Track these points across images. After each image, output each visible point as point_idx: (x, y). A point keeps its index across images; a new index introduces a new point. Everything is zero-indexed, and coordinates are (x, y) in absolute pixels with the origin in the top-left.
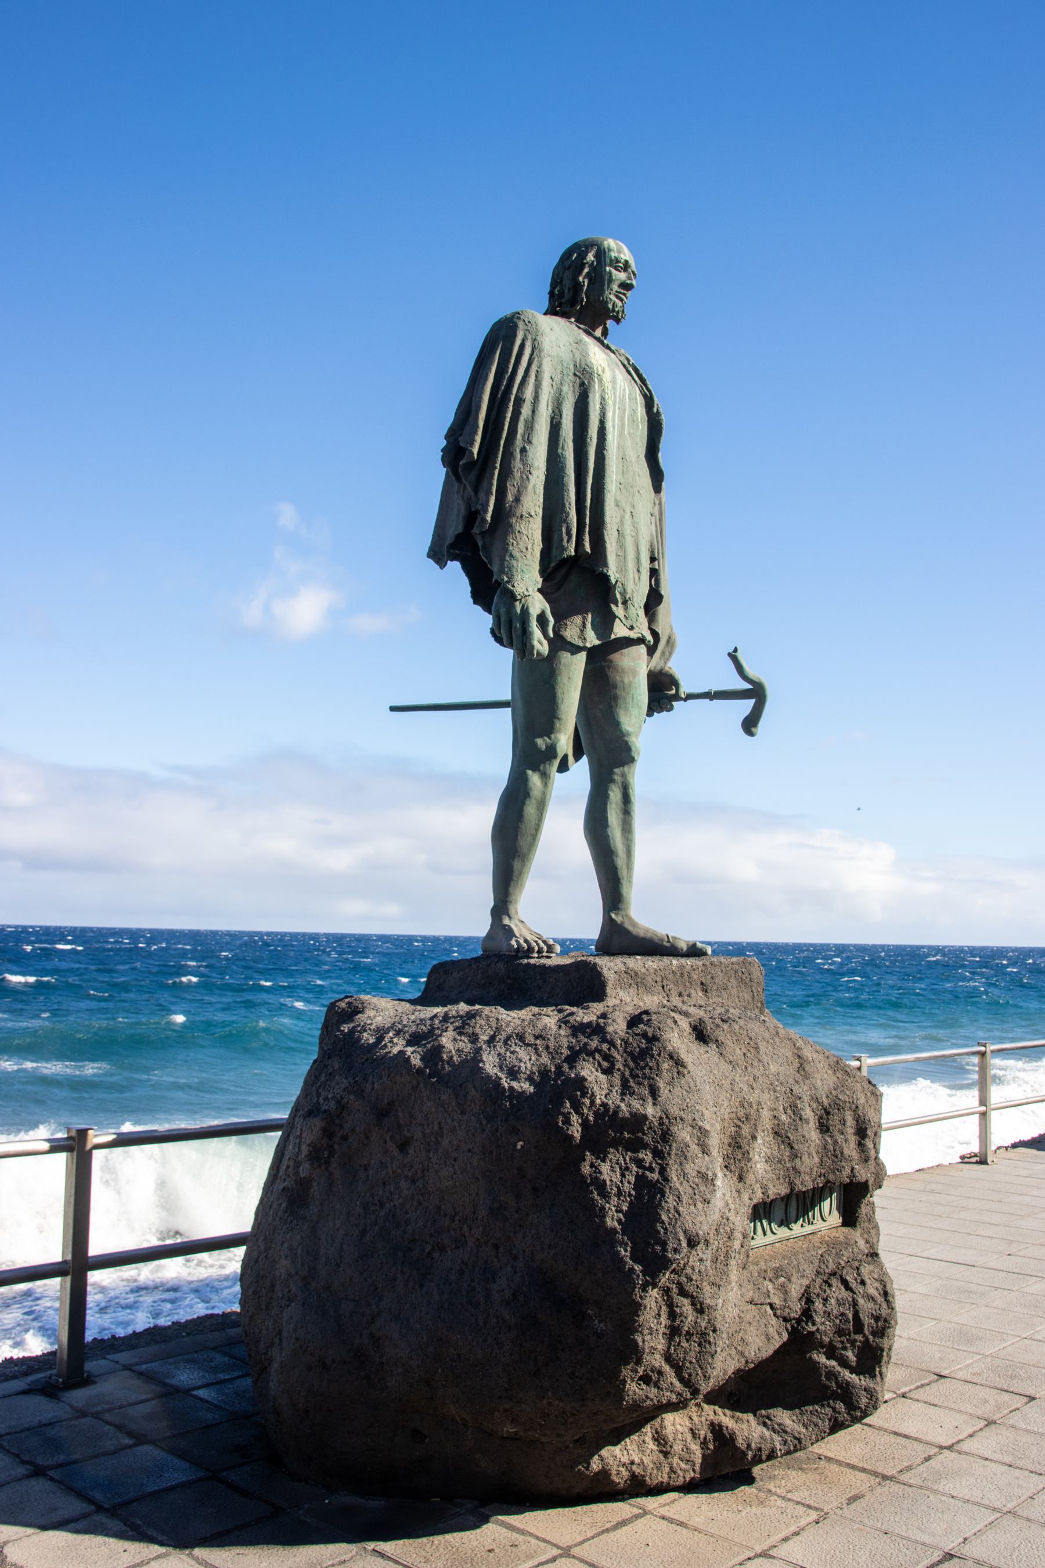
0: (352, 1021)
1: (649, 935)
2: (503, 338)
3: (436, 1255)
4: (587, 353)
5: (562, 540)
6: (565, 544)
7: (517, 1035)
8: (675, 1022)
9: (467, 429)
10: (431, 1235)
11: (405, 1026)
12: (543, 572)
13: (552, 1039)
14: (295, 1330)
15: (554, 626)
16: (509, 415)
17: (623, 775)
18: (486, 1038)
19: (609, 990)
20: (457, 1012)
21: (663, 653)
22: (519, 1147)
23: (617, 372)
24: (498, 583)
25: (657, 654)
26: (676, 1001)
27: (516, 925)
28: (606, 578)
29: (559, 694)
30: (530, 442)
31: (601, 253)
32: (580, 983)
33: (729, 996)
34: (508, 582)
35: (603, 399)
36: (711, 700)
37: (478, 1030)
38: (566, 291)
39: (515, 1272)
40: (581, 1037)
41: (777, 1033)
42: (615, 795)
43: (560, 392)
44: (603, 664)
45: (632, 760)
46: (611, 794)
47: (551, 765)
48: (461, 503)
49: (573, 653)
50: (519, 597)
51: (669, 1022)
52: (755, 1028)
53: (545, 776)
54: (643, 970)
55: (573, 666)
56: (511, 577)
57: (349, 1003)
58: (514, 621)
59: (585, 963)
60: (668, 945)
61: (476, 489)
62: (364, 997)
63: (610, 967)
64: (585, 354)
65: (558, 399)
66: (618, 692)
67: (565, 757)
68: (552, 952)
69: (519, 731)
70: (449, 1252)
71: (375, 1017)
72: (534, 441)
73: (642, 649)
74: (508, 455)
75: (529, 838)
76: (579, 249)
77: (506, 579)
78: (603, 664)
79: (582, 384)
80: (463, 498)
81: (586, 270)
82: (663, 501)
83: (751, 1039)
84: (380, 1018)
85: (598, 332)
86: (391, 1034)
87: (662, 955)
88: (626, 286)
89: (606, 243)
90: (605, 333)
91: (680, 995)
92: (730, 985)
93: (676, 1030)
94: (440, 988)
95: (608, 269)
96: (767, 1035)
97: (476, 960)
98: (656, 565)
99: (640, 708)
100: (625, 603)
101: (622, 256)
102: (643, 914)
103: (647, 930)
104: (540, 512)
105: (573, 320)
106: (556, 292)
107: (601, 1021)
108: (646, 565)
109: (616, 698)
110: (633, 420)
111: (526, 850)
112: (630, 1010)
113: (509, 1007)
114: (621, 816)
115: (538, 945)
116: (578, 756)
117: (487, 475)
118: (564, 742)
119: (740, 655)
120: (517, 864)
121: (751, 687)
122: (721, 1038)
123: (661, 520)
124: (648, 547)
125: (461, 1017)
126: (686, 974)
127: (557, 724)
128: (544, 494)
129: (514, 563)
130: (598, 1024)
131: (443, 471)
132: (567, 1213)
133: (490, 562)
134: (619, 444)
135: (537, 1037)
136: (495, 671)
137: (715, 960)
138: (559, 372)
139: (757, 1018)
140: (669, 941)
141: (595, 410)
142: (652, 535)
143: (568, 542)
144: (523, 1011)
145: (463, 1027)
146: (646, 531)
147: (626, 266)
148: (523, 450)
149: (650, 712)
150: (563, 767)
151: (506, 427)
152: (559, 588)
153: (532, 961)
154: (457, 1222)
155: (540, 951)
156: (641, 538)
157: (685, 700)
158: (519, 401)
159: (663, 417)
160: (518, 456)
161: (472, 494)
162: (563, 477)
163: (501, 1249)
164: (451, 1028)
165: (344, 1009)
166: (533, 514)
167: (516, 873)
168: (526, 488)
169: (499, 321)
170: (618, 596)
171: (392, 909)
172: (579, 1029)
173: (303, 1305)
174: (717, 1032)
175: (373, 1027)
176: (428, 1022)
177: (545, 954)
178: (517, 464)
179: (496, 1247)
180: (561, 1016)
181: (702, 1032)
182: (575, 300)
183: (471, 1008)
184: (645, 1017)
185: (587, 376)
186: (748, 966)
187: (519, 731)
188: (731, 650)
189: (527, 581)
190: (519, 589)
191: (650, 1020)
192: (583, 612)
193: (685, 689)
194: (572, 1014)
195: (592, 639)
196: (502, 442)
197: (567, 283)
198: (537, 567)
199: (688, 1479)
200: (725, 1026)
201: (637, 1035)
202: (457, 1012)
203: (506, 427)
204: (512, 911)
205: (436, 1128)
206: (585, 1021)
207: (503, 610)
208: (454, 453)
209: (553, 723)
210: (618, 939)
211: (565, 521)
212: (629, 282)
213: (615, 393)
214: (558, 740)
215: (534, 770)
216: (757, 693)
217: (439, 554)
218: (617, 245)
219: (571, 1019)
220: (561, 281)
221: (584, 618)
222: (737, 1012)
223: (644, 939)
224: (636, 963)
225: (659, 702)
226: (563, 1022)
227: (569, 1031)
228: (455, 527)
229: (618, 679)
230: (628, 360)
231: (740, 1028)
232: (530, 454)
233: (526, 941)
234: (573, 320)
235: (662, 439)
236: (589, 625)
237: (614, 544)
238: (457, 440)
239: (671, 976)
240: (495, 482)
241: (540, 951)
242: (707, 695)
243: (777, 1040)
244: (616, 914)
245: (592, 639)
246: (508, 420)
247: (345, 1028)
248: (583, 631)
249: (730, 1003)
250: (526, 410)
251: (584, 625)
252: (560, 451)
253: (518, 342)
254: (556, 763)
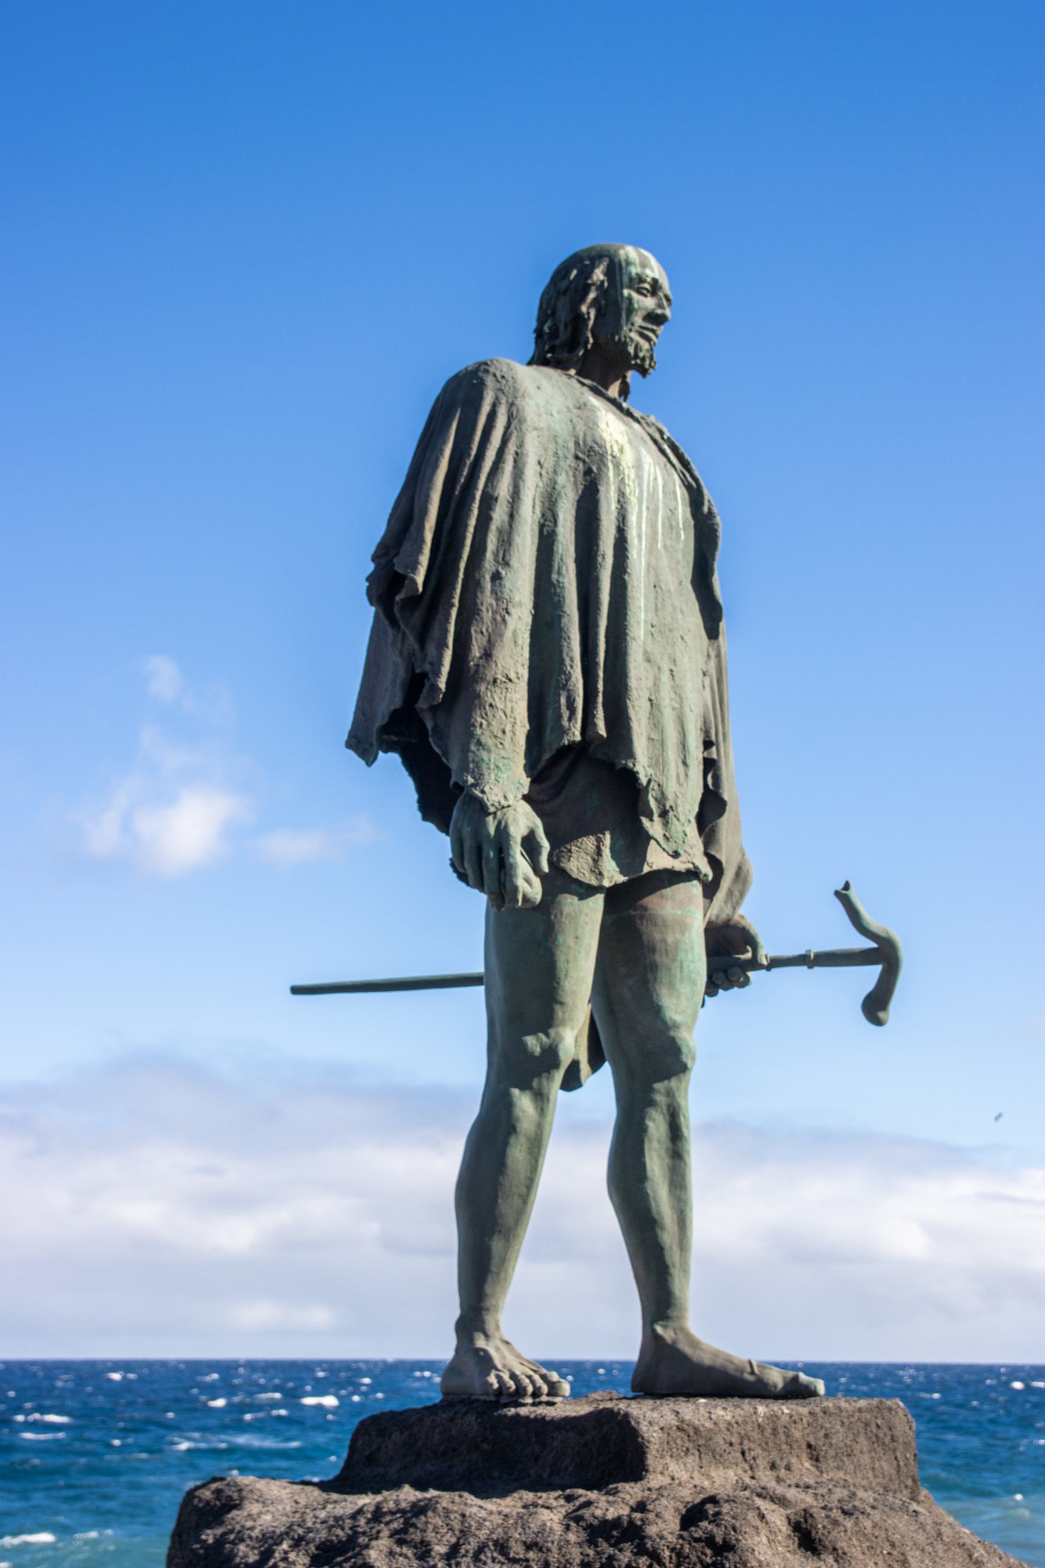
0: (221, 1523)
1: (719, 1363)
2: (462, 401)
4: (595, 424)
5: (560, 717)
6: (565, 723)
7: (496, 1543)
8: (762, 1517)
9: (407, 546)
11: (309, 1530)
12: (530, 767)
13: (555, 1549)
15: (550, 855)
16: (472, 522)
17: (669, 1093)
18: (442, 1549)
19: (651, 1461)
20: (397, 1502)
21: (730, 893)
23: (644, 452)
24: (460, 788)
25: (720, 895)
26: (766, 1478)
27: (497, 1349)
28: (632, 776)
29: (561, 964)
30: (506, 564)
31: (615, 269)
32: (606, 1451)
33: (858, 1467)
34: (474, 785)
35: (621, 494)
36: (810, 967)
37: (430, 1536)
38: (562, 328)
40: (604, 1545)
41: (939, 1534)
42: (656, 1126)
43: (553, 485)
44: (632, 913)
45: (683, 1069)
46: (650, 1124)
47: (550, 1079)
48: (399, 660)
49: (582, 897)
50: (492, 809)
51: (752, 1516)
52: (900, 1524)
53: (541, 1098)
54: (709, 1425)
55: (583, 918)
56: (479, 778)
57: (218, 1492)
58: (485, 846)
59: (610, 1413)
60: (751, 1378)
61: (422, 639)
62: (246, 1480)
63: (652, 1418)
64: (592, 424)
65: (550, 495)
66: (657, 958)
67: (575, 1065)
68: (556, 1395)
69: (498, 1027)
71: (260, 1514)
72: (514, 562)
73: (695, 888)
74: (472, 585)
75: (517, 1201)
76: (581, 263)
77: (471, 780)
78: (632, 913)
79: (588, 472)
80: (401, 654)
81: (592, 295)
82: (723, 651)
83: (893, 1545)
84: (268, 1517)
85: (614, 391)
86: (285, 1546)
87: (742, 1396)
88: (655, 319)
89: (622, 253)
90: (625, 391)
91: (773, 1466)
92: (857, 1448)
93: (764, 1532)
94: (371, 1460)
95: (626, 292)
96: (921, 1538)
97: (431, 1410)
98: (713, 753)
99: (694, 983)
100: (664, 814)
101: (648, 272)
102: (710, 1327)
103: (716, 1354)
104: (525, 673)
105: (573, 372)
106: (546, 329)
107: (637, 1515)
108: (696, 753)
109: (654, 967)
110: (670, 526)
111: (511, 1221)
112: (688, 1495)
113: (483, 1493)
114: (667, 1161)
115: (533, 1382)
116: (595, 1063)
117: (440, 616)
118: (572, 1040)
119: (853, 894)
120: (497, 1245)
121: (874, 945)
122: (842, 1545)
123: (720, 681)
124: (700, 724)
125: (403, 1512)
126: (781, 1430)
127: (559, 1011)
128: (532, 645)
129: (484, 755)
130: (631, 1522)
131: (370, 612)
133: (446, 754)
134: (648, 564)
135: (529, 1547)
136: (459, 928)
137: (829, 1404)
138: (551, 452)
139: (904, 1508)
140: (752, 1373)
141: (609, 512)
142: (706, 706)
143: (570, 720)
144: (509, 1500)
145: (404, 1531)
146: (696, 700)
147: (655, 288)
148: (496, 577)
149: (712, 988)
150: (572, 1081)
151: (468, 542)
152: (556, 794)
153: (523, 1411)
155: (536, 1394)
156: (687, 711)
157: (769, 968)
158: (488, 501)
159: (718, 519)
160: (488, 585)
161: (417, 647)
162: (560, 617)
164: (385, 1533)
165: (208, 1502)
166: (512, 676)
167: (495, 1261)
168: (501, 635)
169: (457, 377)
170: (653, 804)
171: (320, 1316)
172: (601, 1531)
174: (834, 1533)
175: (255, 1533)
176: (348, 1523)
177: (544, 1398)
178: (486, 598)
180: (570, 1507)
181: (809, 1533)
182: (575, 341)
183: (419, 1495)
184: (711, 1509)
185: (596, 458)
186: (886, 1414)
187: (498, 1027)
188: (839, 887)
189: (505, 783)
190: (492, 796)
191: (718, 1514)
192: (595, 831)
193: (767, 951)
194: (588, 1504)
195: (612, 874)
196: (462, 565)
197: (563, 315)
198: (521, 761)
200: (849, 1523)
201: (697, 1540)
202: (397, 1502)
203: (468, 542)
204: (490, 1326)
206: (610, 1516)
207: (467, 831)
208: (387, 585)
209: (552, 1011)
210: (670, 1371)
211: (565, 687)
212: (659, 311)
213: (640, 485)
214: (561, 1038)
215: (522, 1089)
216: (884, 954)
217: (363, 743)
218: (640, 255)
219: (586, 1513)
220: (553, 313)
221: (599, 841)
222: (868, 1496)
223: (711, 1370)
224: (698, 1411)
226: (574, 1518)
227: (583, 1536)
228: (390, 700)
229: (657, 936)
230: (661, 433)
231: (875, 1525)
232: (507, 583)
233: (513, 1376)
234: (573, 372)
235: (719, 555)
236: (606, 852)
237: (644, 721)
238: (390, 564)
239: (755, 1435)
240: (452, 628)
241: (536, 1394)
242: (803, 960)
243: (940, 1547)
244: (665, 1327)
245: (612, 874)
246: (471, 529)
247: (209, 1536)
248: (597, 861)
249: (858, 1481)
250: (499, 515)
251: (599, 852)
252: (554, 576)
253: (486, 409)
254: (559, 1076)
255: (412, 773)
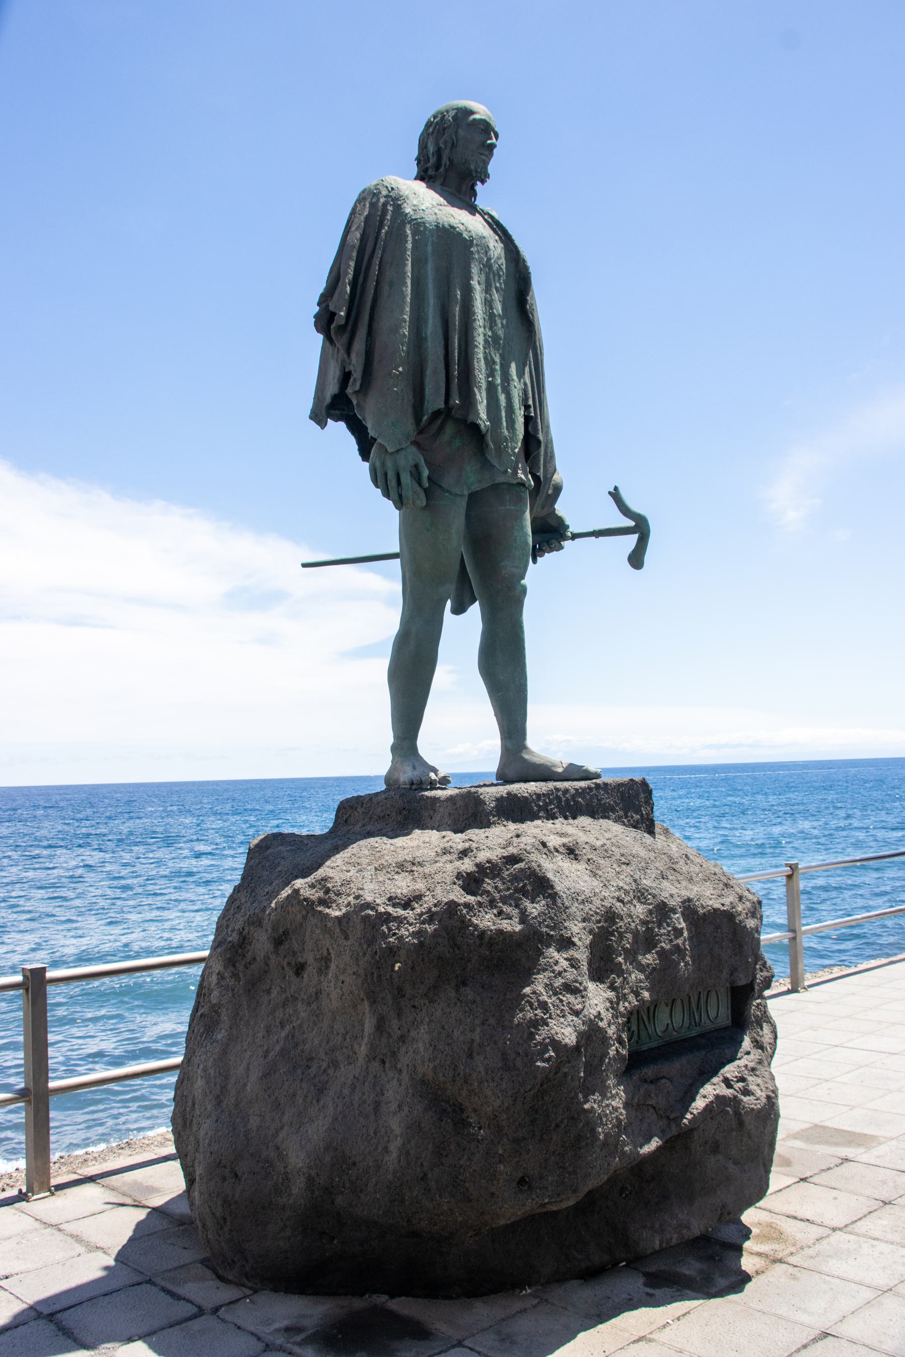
3: (331, 1071)
10: (326, 1054)
14: (209, 1145)
22: (396, 968)
39: (400, 1085)
70: (343, 1069)
132: (443, 1028)
133: (364, 419)
154: (348, 1040)
161: (346, 356)
163: (387, 1065)
173: (217, 1121)
179: (383, 1062)
193: (573, 529)
199: (747, 1043)
205: (325, 953)
216: (640, 528)
217: (320, 415)
225: (548, 542)
228: (332, 388)
238: (328, 306)
255: (353, 434)
